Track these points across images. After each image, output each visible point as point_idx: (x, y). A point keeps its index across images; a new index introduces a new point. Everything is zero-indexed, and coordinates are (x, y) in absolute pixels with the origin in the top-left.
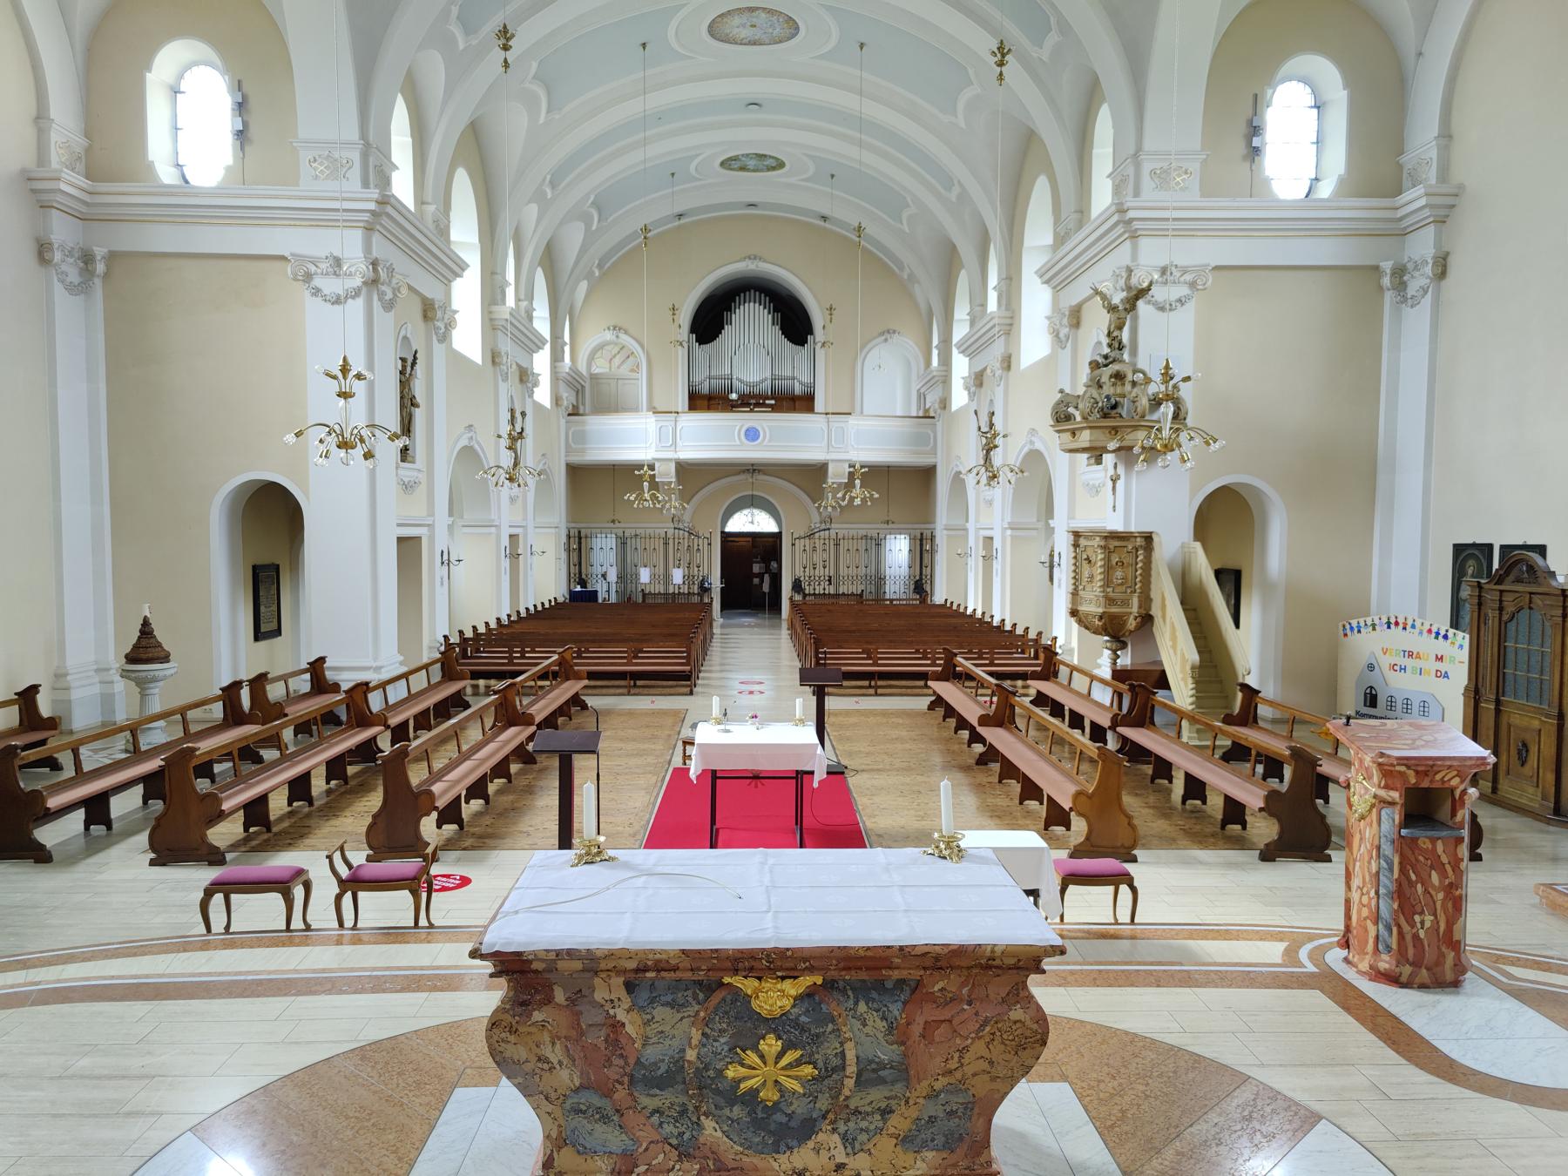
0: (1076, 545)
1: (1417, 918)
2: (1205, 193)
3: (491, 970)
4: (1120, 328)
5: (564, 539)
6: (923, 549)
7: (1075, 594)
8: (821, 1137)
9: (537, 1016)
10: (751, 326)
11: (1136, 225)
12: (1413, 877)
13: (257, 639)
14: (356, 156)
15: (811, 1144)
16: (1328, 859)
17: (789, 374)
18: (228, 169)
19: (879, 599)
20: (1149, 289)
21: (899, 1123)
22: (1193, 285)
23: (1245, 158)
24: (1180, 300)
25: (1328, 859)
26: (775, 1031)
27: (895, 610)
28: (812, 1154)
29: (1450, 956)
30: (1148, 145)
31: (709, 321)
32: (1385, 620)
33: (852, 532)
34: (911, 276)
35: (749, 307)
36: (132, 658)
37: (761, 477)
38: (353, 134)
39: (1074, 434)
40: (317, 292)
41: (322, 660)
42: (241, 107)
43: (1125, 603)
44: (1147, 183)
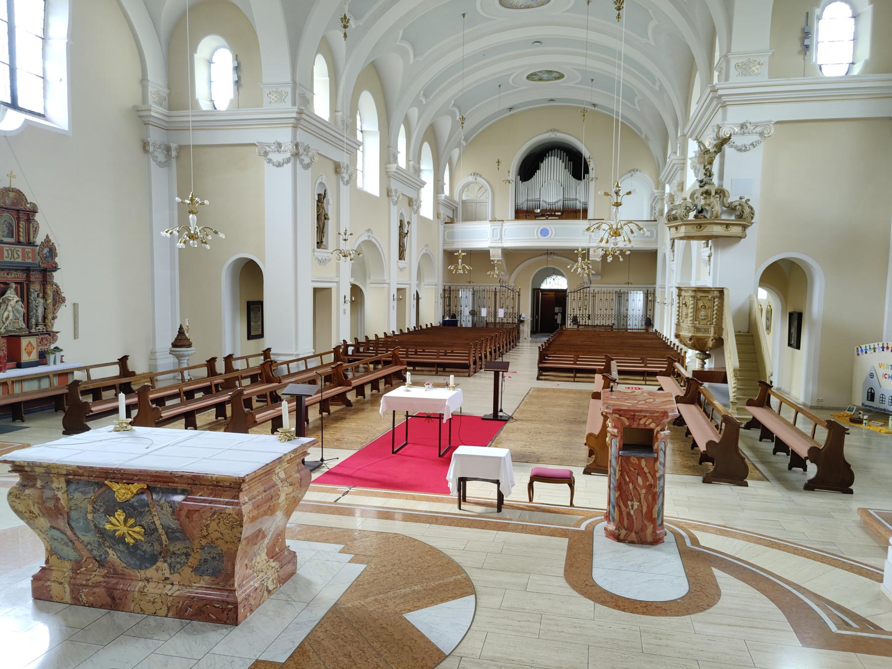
0: (679, 296)
1: (629, 503)
2: (771, 75)
3: (10, 469)
4: (711, 163)
5: (441, 291)
6: (650, 300)
7: (678, 325)
8: (159, 564)
9: (27, 492)
10: (554, 169)
11: (724, 99)
12: (627, 479)
13: (249, 339)
14: (289, 90)
15: (154, 567)
16: (746, 485)
17: (574, 197)
18: (231, 101)
19: (627, 329)
20: (729, 138)
21: (193, 561)
22: (761, 134)
23: (800, 52)
24: (752, 144)
25: (746, 485)
26: (122, 508)
27: (635, 335)
28: (155, 572)
29: (650, 528)
30: (734, 49)
31: (529, 168)
32: (881, 345)
33: (609, 290)
34: (646, 137)
35: (554, 157)
36: (174, 345)
37: (555, 257)
38: (288, 78)
39: (677, 228)
40: (270, 161)
41: (269, 349)
42: (237, 69)
43: (706, 331)
44: (733, 71)
